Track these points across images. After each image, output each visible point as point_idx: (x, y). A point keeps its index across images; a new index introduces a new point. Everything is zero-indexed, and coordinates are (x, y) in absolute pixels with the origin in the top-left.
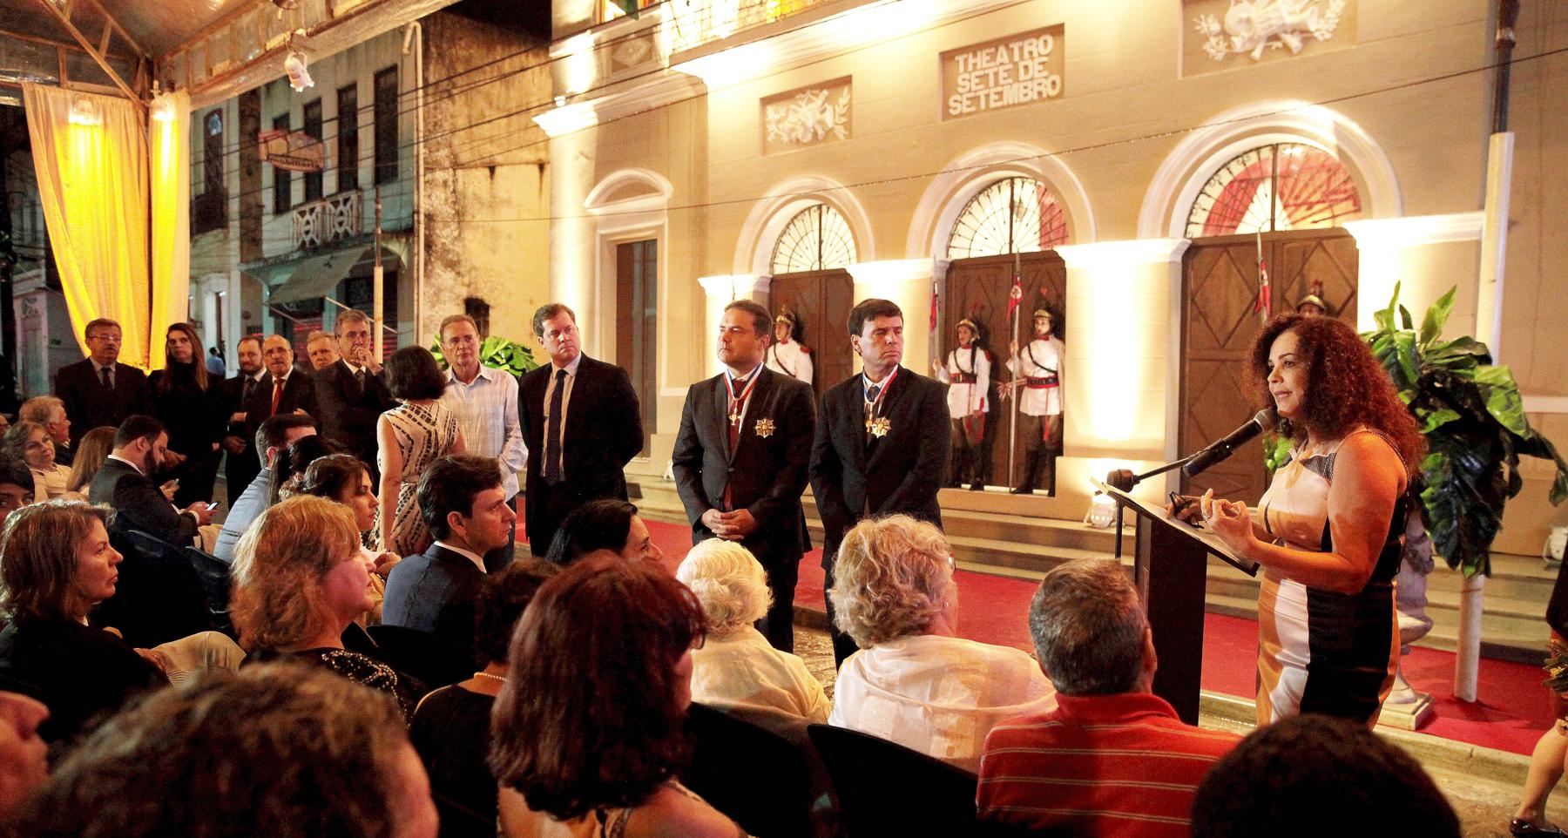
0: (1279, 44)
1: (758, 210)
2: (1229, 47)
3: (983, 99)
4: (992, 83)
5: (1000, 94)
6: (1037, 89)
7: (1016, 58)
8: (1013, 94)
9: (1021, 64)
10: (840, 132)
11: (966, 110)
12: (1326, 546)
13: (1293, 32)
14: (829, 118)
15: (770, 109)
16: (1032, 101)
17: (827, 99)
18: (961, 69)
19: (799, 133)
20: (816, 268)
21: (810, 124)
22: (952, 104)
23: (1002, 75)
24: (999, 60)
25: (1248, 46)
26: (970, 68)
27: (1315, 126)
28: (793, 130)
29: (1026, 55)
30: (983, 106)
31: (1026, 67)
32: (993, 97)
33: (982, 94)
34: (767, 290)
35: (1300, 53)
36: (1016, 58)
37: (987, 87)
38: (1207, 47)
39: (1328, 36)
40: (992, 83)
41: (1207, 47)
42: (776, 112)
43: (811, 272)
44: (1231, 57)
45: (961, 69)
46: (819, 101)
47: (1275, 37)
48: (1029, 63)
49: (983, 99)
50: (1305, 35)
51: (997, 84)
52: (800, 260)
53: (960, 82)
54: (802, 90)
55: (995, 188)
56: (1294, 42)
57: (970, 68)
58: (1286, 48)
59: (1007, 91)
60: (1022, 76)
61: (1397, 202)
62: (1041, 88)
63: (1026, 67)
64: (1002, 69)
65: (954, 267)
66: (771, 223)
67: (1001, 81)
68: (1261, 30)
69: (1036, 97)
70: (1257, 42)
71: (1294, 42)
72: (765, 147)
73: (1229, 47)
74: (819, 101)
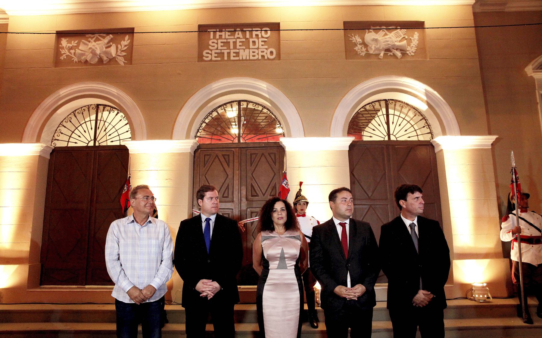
0: (391, 54)
1: (49, 101)
2: (367, 50)
3: (226, 55)
4: (232, 47)
5: (237, 54)
6: (261, 54)
7: (248, 36)
8: (244, 54)
9: (251, 40)
10: (121, 61)
11: (214, 59)
12: (252, 213)
13: (397, 49)
14: (113, 50)
15: (64, 42)
16: (258, 59)
17: (111, 40)
18: (212, 37)
19: (89, 57)
20: (91, 144)
21: (98, 52)
22: (204, 54)
23: (238, 44)
24: (236, 36)
25: (377, 52)
26: (218, 37)
27: (416, 92)
28: (83, 55)
29: (254, 36)
30: (226, 58)
31: (254, 42)
32: (232, 54)
33: (226, 52)
34: (48, 157)
35: (401, 58)
36: (248, 36)
37: (229, 48)
38: (356, 48)
39: (413, 54)
40: (232, 47)
41: (356, 48)
42: (69, 42)
43: (87, 147)
44: (368, 55)
45: (212, 37)
46: (106, 40)
47: (388, 50)
48: (256, 40)
49: (226, 55)
50: (403, 52)
51: (235, 47)
52: (82, 138)
53: (210, 42)
54: (93, 32)
55: (229, 105)
56: (399, 54)
57: (218, 37)
58: (394, 56)
59: (241, 52)
60: (251, 46)
61: (43, 155)
62: (264, 54)
63: (254, 42)
64: (238, 40)
65: (57, 152)
66: (59, 111)
67: (238, 47)
68: (383, 45)
69: (260, 58)
70: (381, 50)
71: (399, 54)
72: (57, 61)
73: (367, 50)
74: (106, 40)
